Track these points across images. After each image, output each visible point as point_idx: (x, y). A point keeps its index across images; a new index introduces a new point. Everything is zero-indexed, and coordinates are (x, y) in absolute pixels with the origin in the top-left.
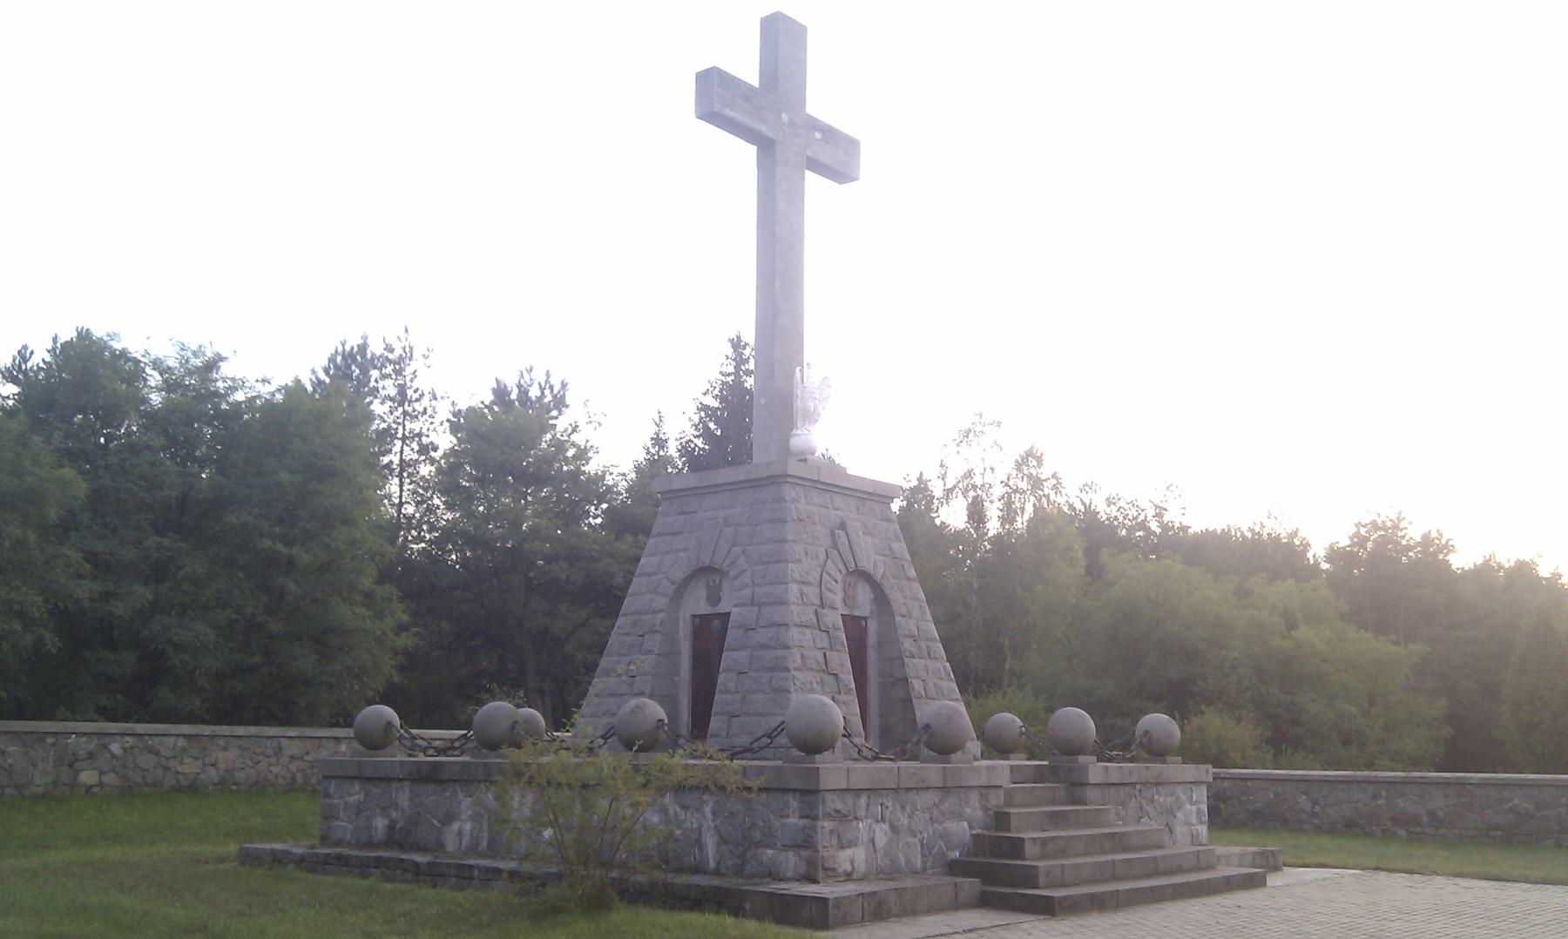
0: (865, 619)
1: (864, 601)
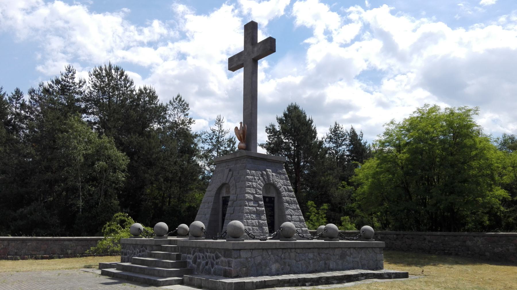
0: (274, 198)
1: (273, 194)
